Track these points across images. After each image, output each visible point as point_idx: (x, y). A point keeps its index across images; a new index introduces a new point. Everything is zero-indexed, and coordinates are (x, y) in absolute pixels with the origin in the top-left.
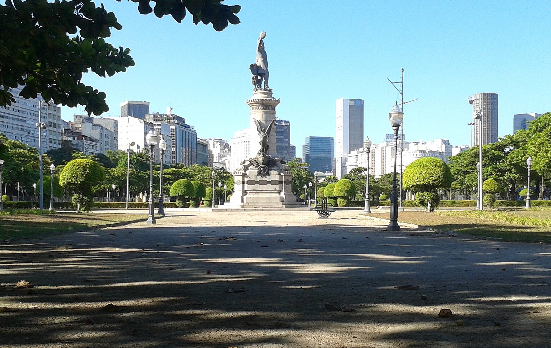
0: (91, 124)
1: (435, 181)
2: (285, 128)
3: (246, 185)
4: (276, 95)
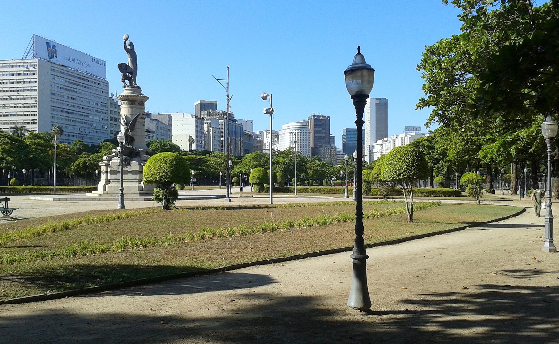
0: (149, 119)
1: (162, 177)
2: (323, 121)
3: (109, 174)
4: (144, 92)
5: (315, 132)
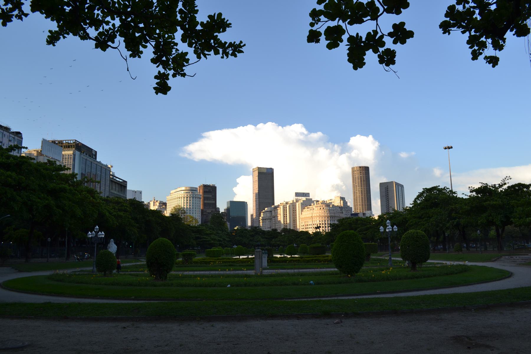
5: (205, 199)
